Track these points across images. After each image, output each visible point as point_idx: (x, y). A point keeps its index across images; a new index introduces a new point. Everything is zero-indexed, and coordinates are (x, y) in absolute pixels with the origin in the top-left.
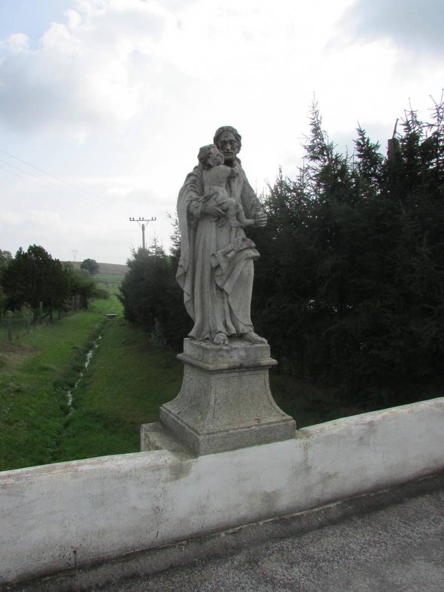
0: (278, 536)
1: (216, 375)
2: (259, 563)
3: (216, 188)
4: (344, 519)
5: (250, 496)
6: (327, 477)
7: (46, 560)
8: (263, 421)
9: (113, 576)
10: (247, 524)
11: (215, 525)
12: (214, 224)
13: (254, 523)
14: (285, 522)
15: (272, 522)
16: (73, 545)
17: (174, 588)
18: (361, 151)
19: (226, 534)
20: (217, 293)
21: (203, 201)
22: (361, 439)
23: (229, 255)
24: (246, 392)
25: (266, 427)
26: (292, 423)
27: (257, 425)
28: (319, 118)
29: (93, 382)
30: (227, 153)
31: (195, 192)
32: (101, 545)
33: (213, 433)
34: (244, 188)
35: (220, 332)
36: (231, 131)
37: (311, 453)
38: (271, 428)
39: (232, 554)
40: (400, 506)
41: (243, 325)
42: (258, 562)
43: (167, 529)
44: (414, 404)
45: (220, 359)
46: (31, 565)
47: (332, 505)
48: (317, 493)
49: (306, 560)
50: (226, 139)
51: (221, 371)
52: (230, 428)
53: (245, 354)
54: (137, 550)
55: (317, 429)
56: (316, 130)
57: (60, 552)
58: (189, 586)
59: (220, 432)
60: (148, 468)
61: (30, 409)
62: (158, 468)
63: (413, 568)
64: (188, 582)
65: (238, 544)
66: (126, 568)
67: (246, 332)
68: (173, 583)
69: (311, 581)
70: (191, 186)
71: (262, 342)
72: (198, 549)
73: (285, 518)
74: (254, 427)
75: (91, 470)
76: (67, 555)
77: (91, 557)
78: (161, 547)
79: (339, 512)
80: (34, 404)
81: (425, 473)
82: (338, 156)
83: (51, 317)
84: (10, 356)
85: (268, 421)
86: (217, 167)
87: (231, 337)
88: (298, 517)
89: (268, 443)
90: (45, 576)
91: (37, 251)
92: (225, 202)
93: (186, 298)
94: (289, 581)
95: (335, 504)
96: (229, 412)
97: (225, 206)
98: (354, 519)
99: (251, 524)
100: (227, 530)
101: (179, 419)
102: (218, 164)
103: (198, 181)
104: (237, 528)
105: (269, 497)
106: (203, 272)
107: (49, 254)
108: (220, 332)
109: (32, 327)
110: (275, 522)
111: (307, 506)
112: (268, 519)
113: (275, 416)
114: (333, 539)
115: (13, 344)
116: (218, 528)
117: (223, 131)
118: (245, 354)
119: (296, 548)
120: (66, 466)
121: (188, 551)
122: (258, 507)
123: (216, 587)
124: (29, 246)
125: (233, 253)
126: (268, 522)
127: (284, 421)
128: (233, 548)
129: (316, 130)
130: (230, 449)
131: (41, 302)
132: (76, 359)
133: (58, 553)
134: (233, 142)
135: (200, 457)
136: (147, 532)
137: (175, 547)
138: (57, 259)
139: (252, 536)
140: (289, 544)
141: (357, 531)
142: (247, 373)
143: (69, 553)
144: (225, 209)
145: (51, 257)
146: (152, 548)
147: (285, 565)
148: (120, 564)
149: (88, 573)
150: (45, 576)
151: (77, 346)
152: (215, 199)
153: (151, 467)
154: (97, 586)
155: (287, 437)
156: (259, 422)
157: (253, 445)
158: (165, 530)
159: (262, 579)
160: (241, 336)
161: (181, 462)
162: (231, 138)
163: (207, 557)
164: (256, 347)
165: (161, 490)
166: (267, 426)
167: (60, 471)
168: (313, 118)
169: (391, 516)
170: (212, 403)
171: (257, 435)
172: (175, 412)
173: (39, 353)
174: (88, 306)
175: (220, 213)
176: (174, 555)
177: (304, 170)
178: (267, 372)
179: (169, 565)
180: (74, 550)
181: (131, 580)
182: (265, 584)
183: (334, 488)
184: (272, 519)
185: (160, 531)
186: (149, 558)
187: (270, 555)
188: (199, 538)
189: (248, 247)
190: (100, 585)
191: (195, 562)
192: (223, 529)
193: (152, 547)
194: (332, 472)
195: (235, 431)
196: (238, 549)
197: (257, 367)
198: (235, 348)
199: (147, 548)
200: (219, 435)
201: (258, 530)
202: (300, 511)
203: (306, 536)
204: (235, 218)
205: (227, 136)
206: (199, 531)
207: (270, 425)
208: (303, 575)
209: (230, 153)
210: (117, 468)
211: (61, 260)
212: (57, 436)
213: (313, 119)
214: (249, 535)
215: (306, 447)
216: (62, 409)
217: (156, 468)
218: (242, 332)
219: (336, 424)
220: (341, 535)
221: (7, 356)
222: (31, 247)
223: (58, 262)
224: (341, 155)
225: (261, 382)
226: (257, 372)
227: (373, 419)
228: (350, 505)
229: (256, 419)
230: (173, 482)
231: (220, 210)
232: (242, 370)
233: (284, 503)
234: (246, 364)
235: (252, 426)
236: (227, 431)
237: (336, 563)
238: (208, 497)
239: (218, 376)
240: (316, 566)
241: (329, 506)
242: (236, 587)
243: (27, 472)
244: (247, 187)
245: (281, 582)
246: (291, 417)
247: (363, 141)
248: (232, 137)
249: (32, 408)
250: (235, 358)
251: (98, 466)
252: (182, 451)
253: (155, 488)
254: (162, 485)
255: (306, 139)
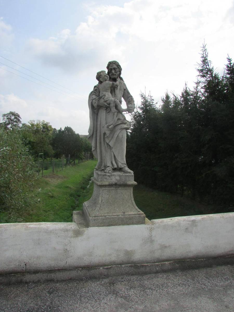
0: (131, 273)
1: (103, 188)
2: (115, 284)
3: (104, 93)
4: (172, 270)
5: (117, 251)
6: (164, 247)
7: (12, 266)
8: (126, 213)
9: (42, 278)
10: (115, 265)
11: (97, 263)
12: (105, 111)
13: (119, 265)
14: (137, 267)
15: (130, 266)
16: (25, 261)
17: (67, 288)
18: (228, 70)
19: (103, 268)
20: (107, 147)
21: (98, 100)
22: (187, 229)
23: (110, 127)
24: (119, 198)
25: (128, 217)
26: (143, 216)
27: (123, 215)
28: (207, 54)
29: (88, 195)
30: (113, 74)
31: (96, 95)
32: (38, 263)
33: (97, 217)
34: (124, 92)
35: (108, 166)
36: (114, 63)
37: (154, 233)
38: (130, 217)
39: (103, 278)
40: (209, 268)
41: (121, 164)
42: (114, 284)
43: (71, 261)
44: (225, 214)
45: (105, 180)
46: (5, 267)
47: (167, 263)
48: (157, 255)
49: (140, 287)
50: (112, 68)
51: (105, 186)
52: (107, 215)
53: (119, 178)
54: (56, 269)
55: (160, 221)
56: (205, 61)
57: (19, 264)
58: (74, 289)
59: (101, 216)
60: (62, 230)
61: (56, 206)
62: (67, 230)
63: (198, 300)
64: (75, 287)
65: (108, 274)
66: (49, 276)
67: (122, 167)
68: (68, 286)
69: (137, 297)
70: (94, 93)
71: (130, 173)
72: (86, 273)
73: (137, 265)
74: (120, 216)
75: (34, 227)
76: (22, 265)
77: (33, 269)
78: (68, 269)
79: (170, 267)
80: (59, 203)
81: (231, 253)
82: (216, 74)
83: (74, 163)
84: (52, 180)
85: (130, 213)
86: (105, 82)
87: (115, 170)
88: (145, 266)
89: (128, 225)
90: (12, 273)
91: (68, 129)
92: (108, 100)
93: (93, 149)
94: (125, 295)
95: (169, 262)
96: (109, 207)
97: (108, 102)
98: (178, 271)
99: (117, 266)
100: (104, 266)
101: (87, 209)
102: (106, 80)
103: (98, 90)
104: (110, 266)
105: (128, 253)
106: (100, 136)
107: (74, 131)
108: (108, 166)
109: (64, 167)
110: (131, 266)
111: (151, 260)
112: (128, 264)
113: (135, 211)
114: (160, 279)
115: (54, 175)
116: (99, 265)
117: (111, 63)
118: (119, 178)
119: (138, 280)
120: (23, 225)
121: (81, 273)
122: (122, 257)
123: (87, 292)
124: (65, 127)
125: (112, 126)
126: (128, 266)
127: (139, 214)
128: (105, 275)
129: (205, 61)
130: (107, 225)
131: (69, 155)
132: (83, 183)
133: (17, 264)
134: (116, 69)
135: (89, 228)
136: (61, 261)
137: (75, 270)
138: (78, 133)
139: (117, 271)
140: (135, 278)
141: (176, 278)
142: (120, 188)
143: (23, 265)
144: (108, 103)
145: (75, 132)
146: (64, 269)
147: (127, 287)
148: (47, 274)
149: (31, 275)
150: (12, 273)
151: (85, 177)
152: (103, 98)
153: (63, 230)
154: (33, 282)
155: (140, 223)
156: (124, 214)
157: (119, 225)
158: (70, 261)
159: (112, 292)
160: (120, 169)
161: (79, 229)
162: (114, 67)
163: (90, 277)
164: (125, 175)
165: (68, 241)
166: (128, 216)
167: (20, 226)
168: (202, 54)
169: (200, 274)
170: (100, 201)
171: (122, 220)
172: (87, 206)
173: (65, 179)
174: (94, 157)
175: (106, 105)
176: (74, 274)
177: (198, 83)
178: (132, 189)
179: (70, 278)
180: (25, 263)
181: (49, 282)
182: (113, 294)
183: (167, 254)
184: (130, 265)
185: (67, 261)
186: (61, 273)
187: (122, 281)
188: (88, 268)
189: (121, 123)
190: (35, 282)
191: (83, 279)
192: (101, 266)
193: (64, 268)
194: (167, 245)
195: (109, 217)
196: (107, 276)
197: (125, 185)
198: (114, 175)
199: (61, 268)
200: (101, 218)
201: (121, 269)
202: (147, 263)
203: (147, 276)
204: (114, 108)
205: (112, 66)
206: (88, 265)
207: (130, 216)
208: (135, 294)
209: (114, 74)
210: (46, 228)
211: (80, 134)
212: (67, 220)
213: (203, 54)
214: (115, 270)
215: (151, 230)
216: (72, 207)
217: (66, 230)
218: (120, 167)
219: (171, 220)
220: (166, 278)
221: (50, 180)
222: (66, 127)
223: (78, 135)
224: (218, 74)
225: (128, 194)
226: (126, 188)
227: (195, 219)
228: (178, 264)
229: (123, 212)
230: (74, 238)
231: (106, 104)
232: (117, 186)
233: (138, 256)
234: (118, 183)
235: (119, 215)
236: (105, 216)
237: (155, 291)
238: (93, 248)
239: (103, 188)
240: (144, 290)
241: (165, 263)
242: (97, 293)
243: (6, 225)
244: (126, 92)
245: (121, 295)
246: (143, 213)
247: (230, 65)
248: (115, 66)
249: (57, 205)
250: (113, 180)
251: (38, 226)
252: (84, 224)
253: (65, 240)
254: (69, 239)
255: (198, 66)
